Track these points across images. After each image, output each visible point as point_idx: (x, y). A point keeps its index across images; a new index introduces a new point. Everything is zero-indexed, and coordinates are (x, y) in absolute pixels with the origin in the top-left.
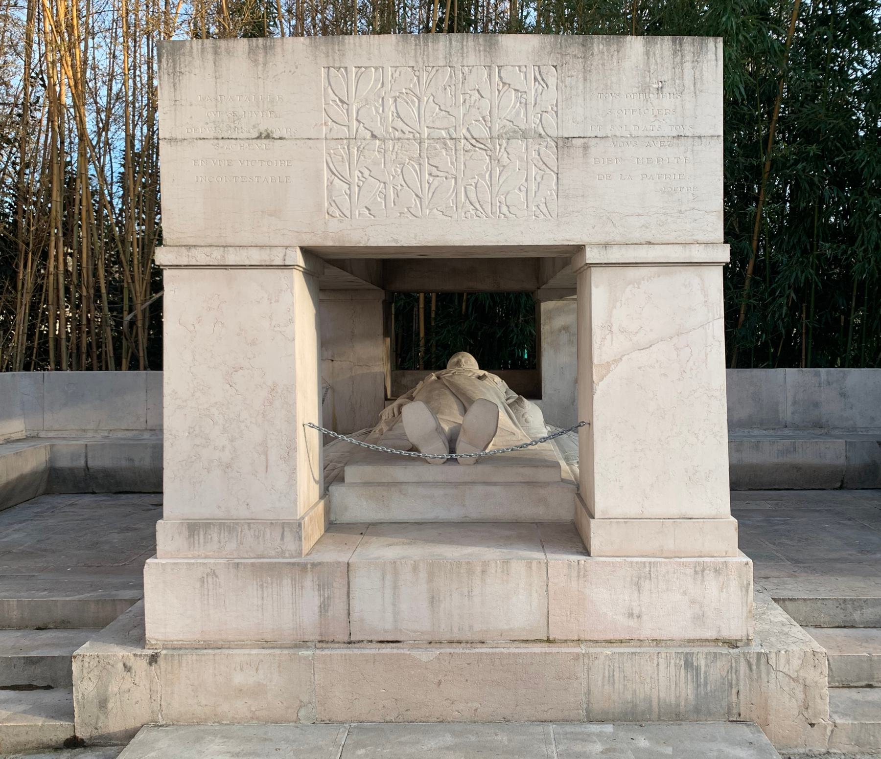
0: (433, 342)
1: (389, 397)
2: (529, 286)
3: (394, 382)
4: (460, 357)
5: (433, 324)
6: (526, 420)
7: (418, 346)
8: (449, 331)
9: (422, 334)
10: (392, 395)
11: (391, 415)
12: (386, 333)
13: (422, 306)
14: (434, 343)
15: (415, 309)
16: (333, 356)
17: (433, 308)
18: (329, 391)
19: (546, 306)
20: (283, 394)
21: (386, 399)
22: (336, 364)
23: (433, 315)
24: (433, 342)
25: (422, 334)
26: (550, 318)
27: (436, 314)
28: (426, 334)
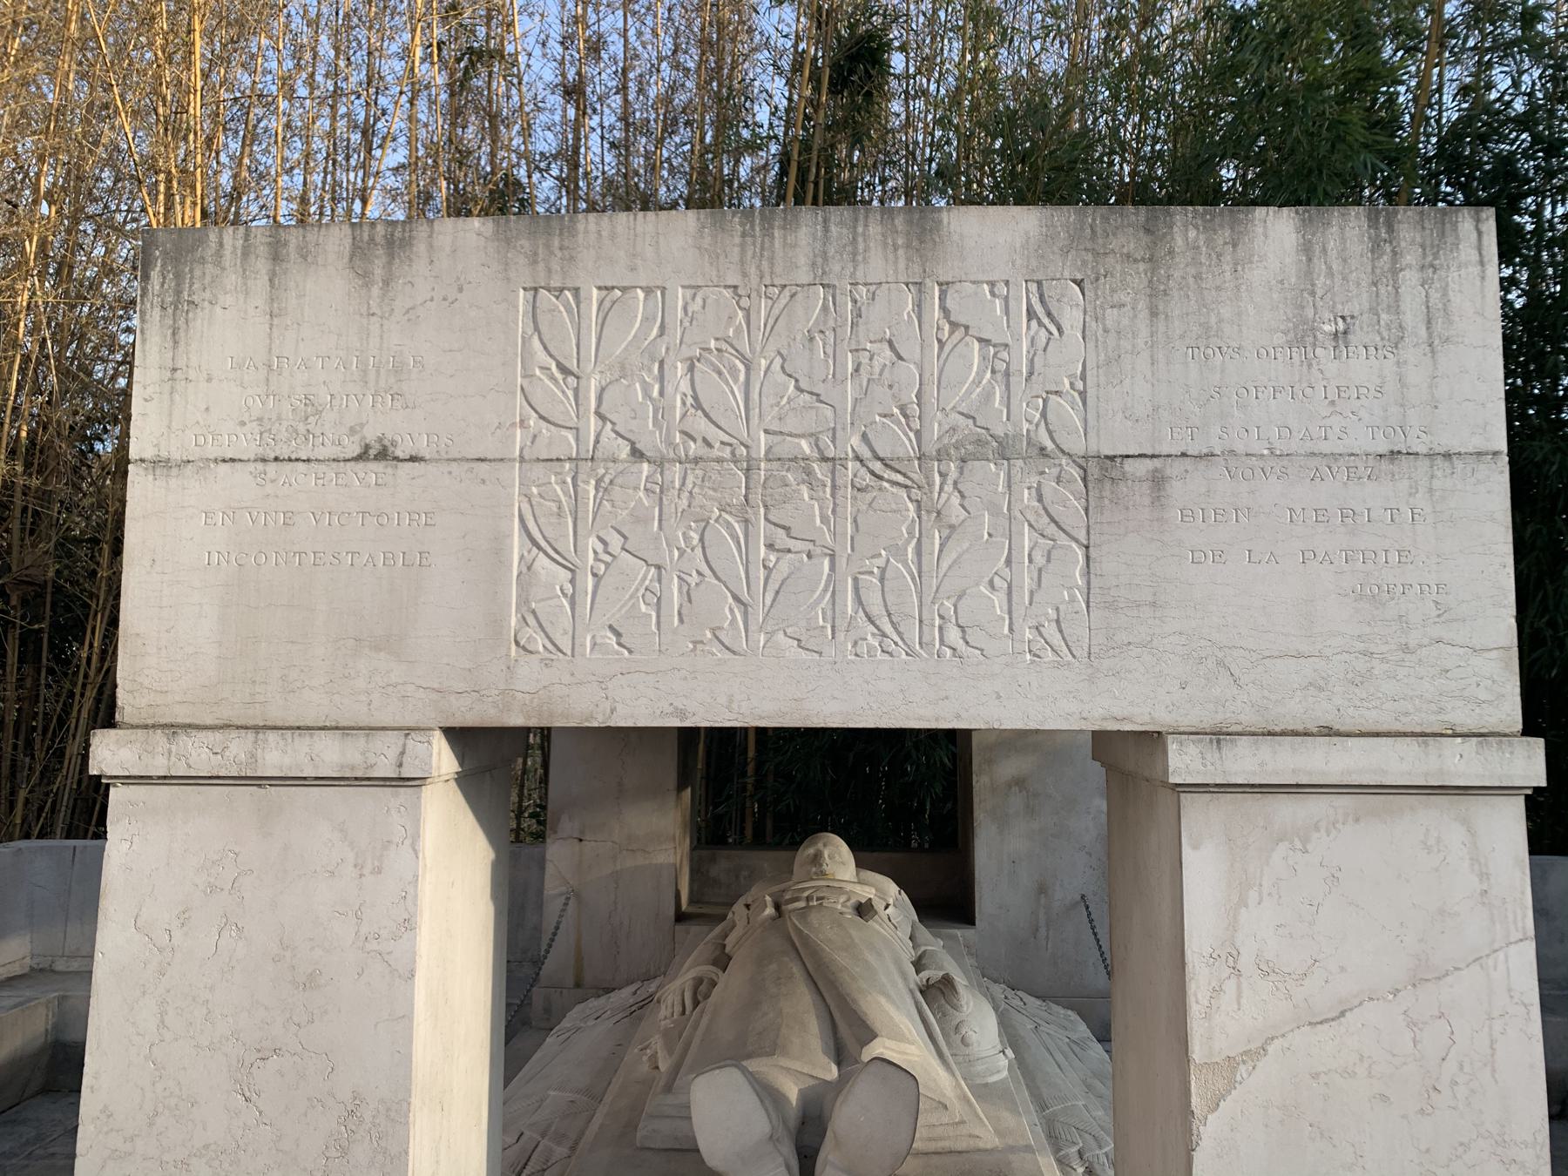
3: (694, 872)
4: (820, 845)
9: (751, 753)
10: (691, 901)
11: (678, 1009)
12: (683, 782)
16: (582, 832)
21: (680, 917)
25: (751, 753)
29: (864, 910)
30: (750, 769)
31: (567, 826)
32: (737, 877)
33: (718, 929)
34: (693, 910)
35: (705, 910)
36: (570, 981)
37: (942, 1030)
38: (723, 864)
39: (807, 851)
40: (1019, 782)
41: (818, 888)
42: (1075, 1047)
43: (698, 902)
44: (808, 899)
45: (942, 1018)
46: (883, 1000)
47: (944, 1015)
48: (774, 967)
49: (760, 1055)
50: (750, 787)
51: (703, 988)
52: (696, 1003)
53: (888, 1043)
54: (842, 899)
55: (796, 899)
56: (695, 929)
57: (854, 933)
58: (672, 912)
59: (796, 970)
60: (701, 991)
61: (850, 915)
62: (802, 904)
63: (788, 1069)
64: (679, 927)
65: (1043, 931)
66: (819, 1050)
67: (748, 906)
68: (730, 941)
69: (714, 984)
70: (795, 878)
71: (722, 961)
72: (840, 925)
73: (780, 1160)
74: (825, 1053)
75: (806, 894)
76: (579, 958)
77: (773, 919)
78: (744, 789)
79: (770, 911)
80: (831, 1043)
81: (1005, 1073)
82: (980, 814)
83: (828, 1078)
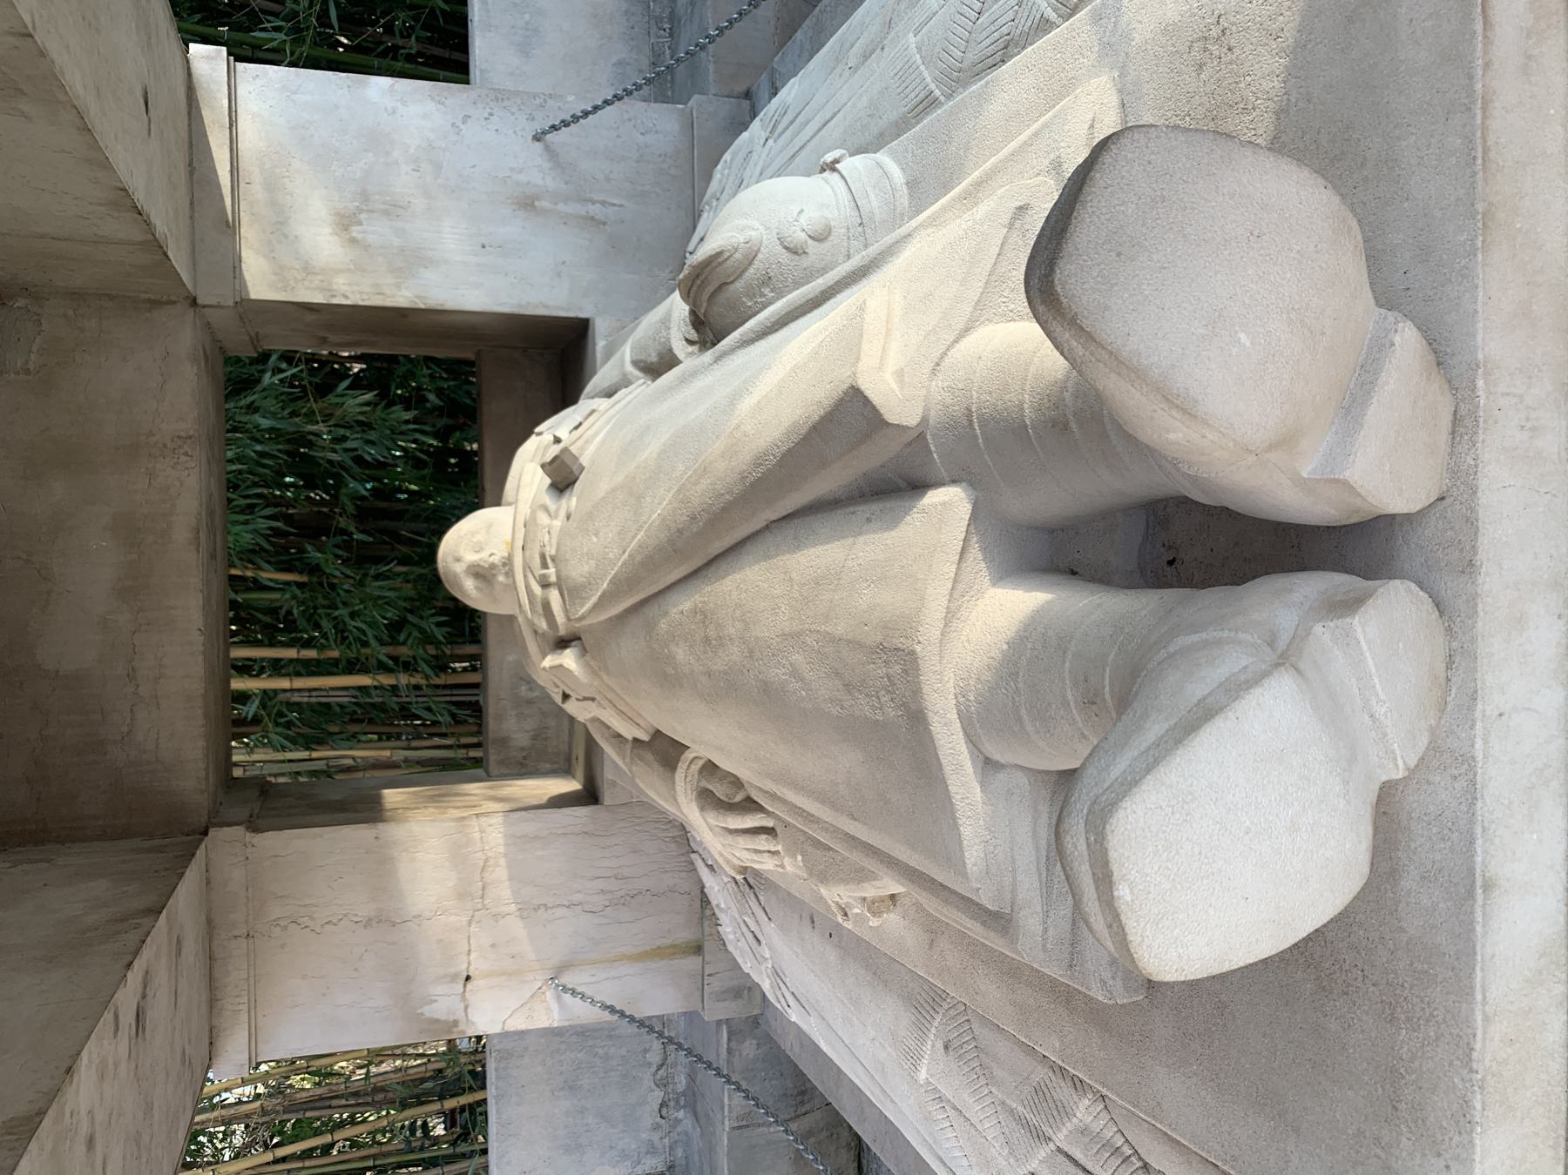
0: (382, 653)
1: (571, 785)
2: (185, 336)
3: (524, 768)
4: (459, 568)
5: (335, 654)
6: (820, 237)
7: (394, 688)
8: (353, 615)
9: (365, 680)
10: (566, 771)
11: (762, 842)
12: (367, 810)
13: (284, 683)
14: (385, 650)
15: (296, 698)
16: (453, 978)
17: (291, 653)
18: (569, 979)
19: (261, 279)
20: (414, 793)
21: (590, 796)
22: (478, 965)
23: (311, 654)
24: (382, 653)
25: (365, 680)
26: (308, 269)
27: (307, 644)
28: (365, 670)
29: (563, 477)
30: (386, 680)
31: (443, 1004)
32: (530, 702)
33: (609, 750)
34: (580, 771)
35: (580, 751)
36: (693, 962)
37: (797, 284)
38: (508, 724)
39: (470, 592)
40: (345, 223)
41: (527, 567)
42: (780, 128)
43: (569, 760)
44: (545, 585)
45: (771, 284)
46: (747, 404)
47: (767, 280)
48: (681, 653)
49: (917, 692)
50: (413, 681)
51: (720, 790)
52: (750, 805)
53: (868, 360)
54: (543, 519)
55: (546, 606)
56: (608, 775)
57: (603, 487)
58: (582, 812)
59: (683, 604)
60: (727, 795)
61: (572, 501)
62: (554, 596)
63: (950, 615)
64: (607, 799)
65: (595, 210)
66: (892, 537)
67: (566, 697)
68: (629, 732)
69: (710, 768)
70: (516, 611)
71: (664, 751)
72: (590, 516)
73: (1323, 633)
74: (894, 523)
75: (537, 590)
76: (658, 953)
77: (584, 651)
78: (417, 687)
79: (568, 659)
80: (863, 510)
81: (882, 157)
82: (401, 296)
83: (965, 509)
